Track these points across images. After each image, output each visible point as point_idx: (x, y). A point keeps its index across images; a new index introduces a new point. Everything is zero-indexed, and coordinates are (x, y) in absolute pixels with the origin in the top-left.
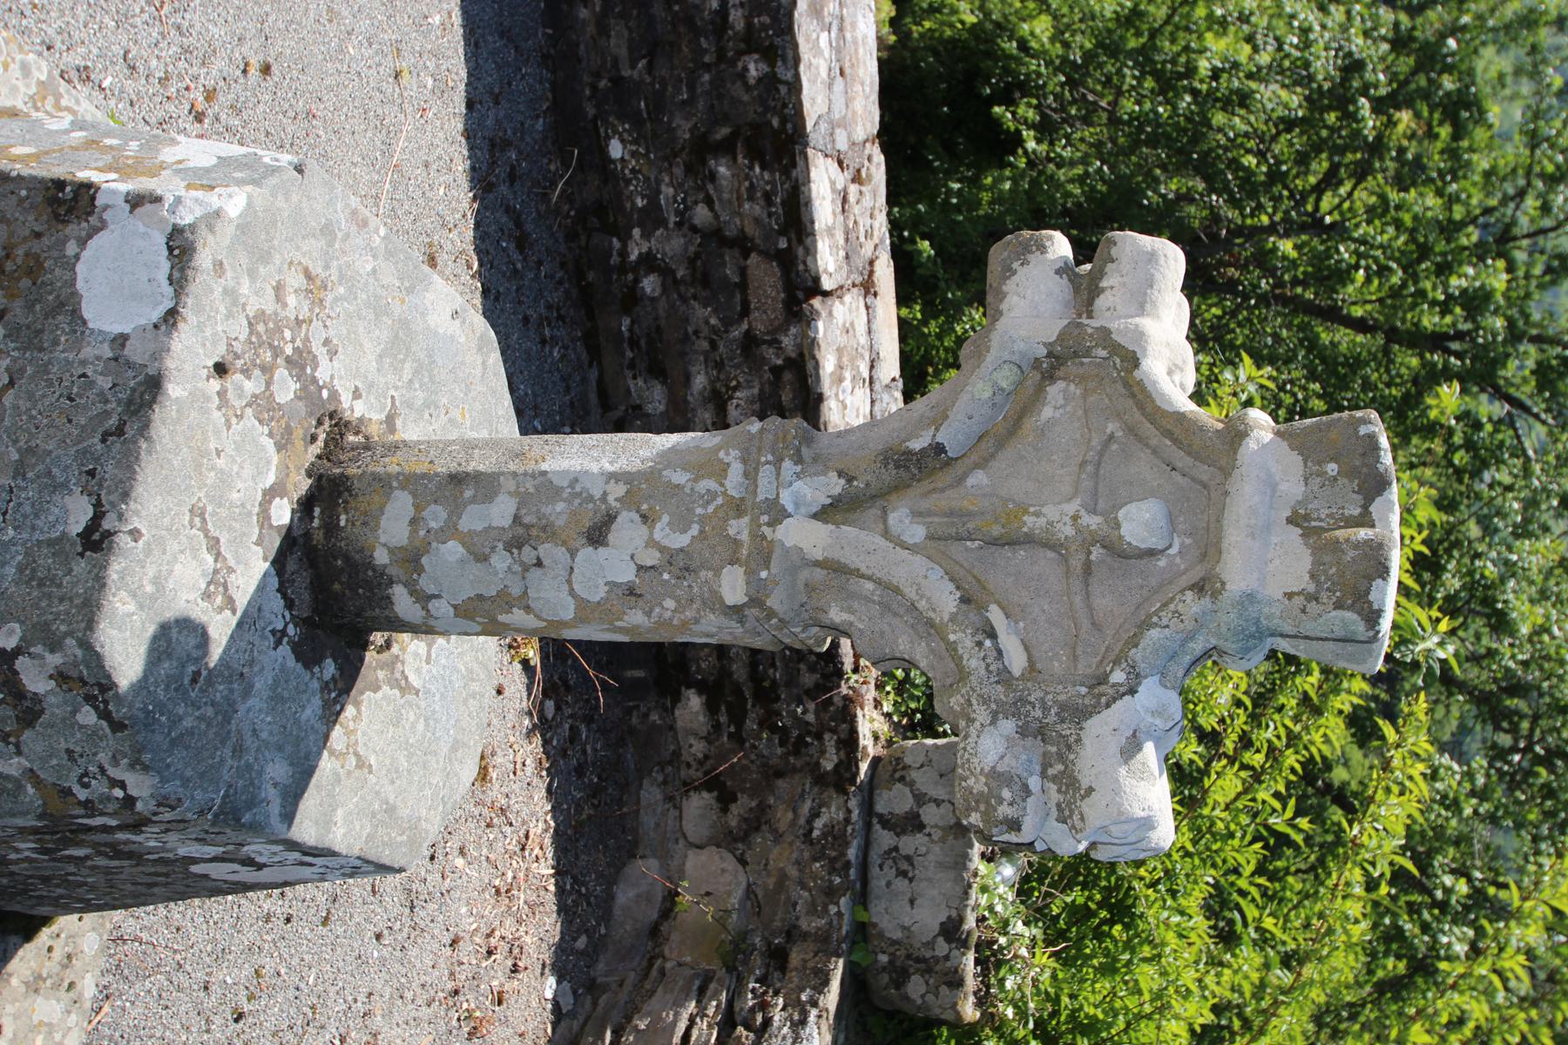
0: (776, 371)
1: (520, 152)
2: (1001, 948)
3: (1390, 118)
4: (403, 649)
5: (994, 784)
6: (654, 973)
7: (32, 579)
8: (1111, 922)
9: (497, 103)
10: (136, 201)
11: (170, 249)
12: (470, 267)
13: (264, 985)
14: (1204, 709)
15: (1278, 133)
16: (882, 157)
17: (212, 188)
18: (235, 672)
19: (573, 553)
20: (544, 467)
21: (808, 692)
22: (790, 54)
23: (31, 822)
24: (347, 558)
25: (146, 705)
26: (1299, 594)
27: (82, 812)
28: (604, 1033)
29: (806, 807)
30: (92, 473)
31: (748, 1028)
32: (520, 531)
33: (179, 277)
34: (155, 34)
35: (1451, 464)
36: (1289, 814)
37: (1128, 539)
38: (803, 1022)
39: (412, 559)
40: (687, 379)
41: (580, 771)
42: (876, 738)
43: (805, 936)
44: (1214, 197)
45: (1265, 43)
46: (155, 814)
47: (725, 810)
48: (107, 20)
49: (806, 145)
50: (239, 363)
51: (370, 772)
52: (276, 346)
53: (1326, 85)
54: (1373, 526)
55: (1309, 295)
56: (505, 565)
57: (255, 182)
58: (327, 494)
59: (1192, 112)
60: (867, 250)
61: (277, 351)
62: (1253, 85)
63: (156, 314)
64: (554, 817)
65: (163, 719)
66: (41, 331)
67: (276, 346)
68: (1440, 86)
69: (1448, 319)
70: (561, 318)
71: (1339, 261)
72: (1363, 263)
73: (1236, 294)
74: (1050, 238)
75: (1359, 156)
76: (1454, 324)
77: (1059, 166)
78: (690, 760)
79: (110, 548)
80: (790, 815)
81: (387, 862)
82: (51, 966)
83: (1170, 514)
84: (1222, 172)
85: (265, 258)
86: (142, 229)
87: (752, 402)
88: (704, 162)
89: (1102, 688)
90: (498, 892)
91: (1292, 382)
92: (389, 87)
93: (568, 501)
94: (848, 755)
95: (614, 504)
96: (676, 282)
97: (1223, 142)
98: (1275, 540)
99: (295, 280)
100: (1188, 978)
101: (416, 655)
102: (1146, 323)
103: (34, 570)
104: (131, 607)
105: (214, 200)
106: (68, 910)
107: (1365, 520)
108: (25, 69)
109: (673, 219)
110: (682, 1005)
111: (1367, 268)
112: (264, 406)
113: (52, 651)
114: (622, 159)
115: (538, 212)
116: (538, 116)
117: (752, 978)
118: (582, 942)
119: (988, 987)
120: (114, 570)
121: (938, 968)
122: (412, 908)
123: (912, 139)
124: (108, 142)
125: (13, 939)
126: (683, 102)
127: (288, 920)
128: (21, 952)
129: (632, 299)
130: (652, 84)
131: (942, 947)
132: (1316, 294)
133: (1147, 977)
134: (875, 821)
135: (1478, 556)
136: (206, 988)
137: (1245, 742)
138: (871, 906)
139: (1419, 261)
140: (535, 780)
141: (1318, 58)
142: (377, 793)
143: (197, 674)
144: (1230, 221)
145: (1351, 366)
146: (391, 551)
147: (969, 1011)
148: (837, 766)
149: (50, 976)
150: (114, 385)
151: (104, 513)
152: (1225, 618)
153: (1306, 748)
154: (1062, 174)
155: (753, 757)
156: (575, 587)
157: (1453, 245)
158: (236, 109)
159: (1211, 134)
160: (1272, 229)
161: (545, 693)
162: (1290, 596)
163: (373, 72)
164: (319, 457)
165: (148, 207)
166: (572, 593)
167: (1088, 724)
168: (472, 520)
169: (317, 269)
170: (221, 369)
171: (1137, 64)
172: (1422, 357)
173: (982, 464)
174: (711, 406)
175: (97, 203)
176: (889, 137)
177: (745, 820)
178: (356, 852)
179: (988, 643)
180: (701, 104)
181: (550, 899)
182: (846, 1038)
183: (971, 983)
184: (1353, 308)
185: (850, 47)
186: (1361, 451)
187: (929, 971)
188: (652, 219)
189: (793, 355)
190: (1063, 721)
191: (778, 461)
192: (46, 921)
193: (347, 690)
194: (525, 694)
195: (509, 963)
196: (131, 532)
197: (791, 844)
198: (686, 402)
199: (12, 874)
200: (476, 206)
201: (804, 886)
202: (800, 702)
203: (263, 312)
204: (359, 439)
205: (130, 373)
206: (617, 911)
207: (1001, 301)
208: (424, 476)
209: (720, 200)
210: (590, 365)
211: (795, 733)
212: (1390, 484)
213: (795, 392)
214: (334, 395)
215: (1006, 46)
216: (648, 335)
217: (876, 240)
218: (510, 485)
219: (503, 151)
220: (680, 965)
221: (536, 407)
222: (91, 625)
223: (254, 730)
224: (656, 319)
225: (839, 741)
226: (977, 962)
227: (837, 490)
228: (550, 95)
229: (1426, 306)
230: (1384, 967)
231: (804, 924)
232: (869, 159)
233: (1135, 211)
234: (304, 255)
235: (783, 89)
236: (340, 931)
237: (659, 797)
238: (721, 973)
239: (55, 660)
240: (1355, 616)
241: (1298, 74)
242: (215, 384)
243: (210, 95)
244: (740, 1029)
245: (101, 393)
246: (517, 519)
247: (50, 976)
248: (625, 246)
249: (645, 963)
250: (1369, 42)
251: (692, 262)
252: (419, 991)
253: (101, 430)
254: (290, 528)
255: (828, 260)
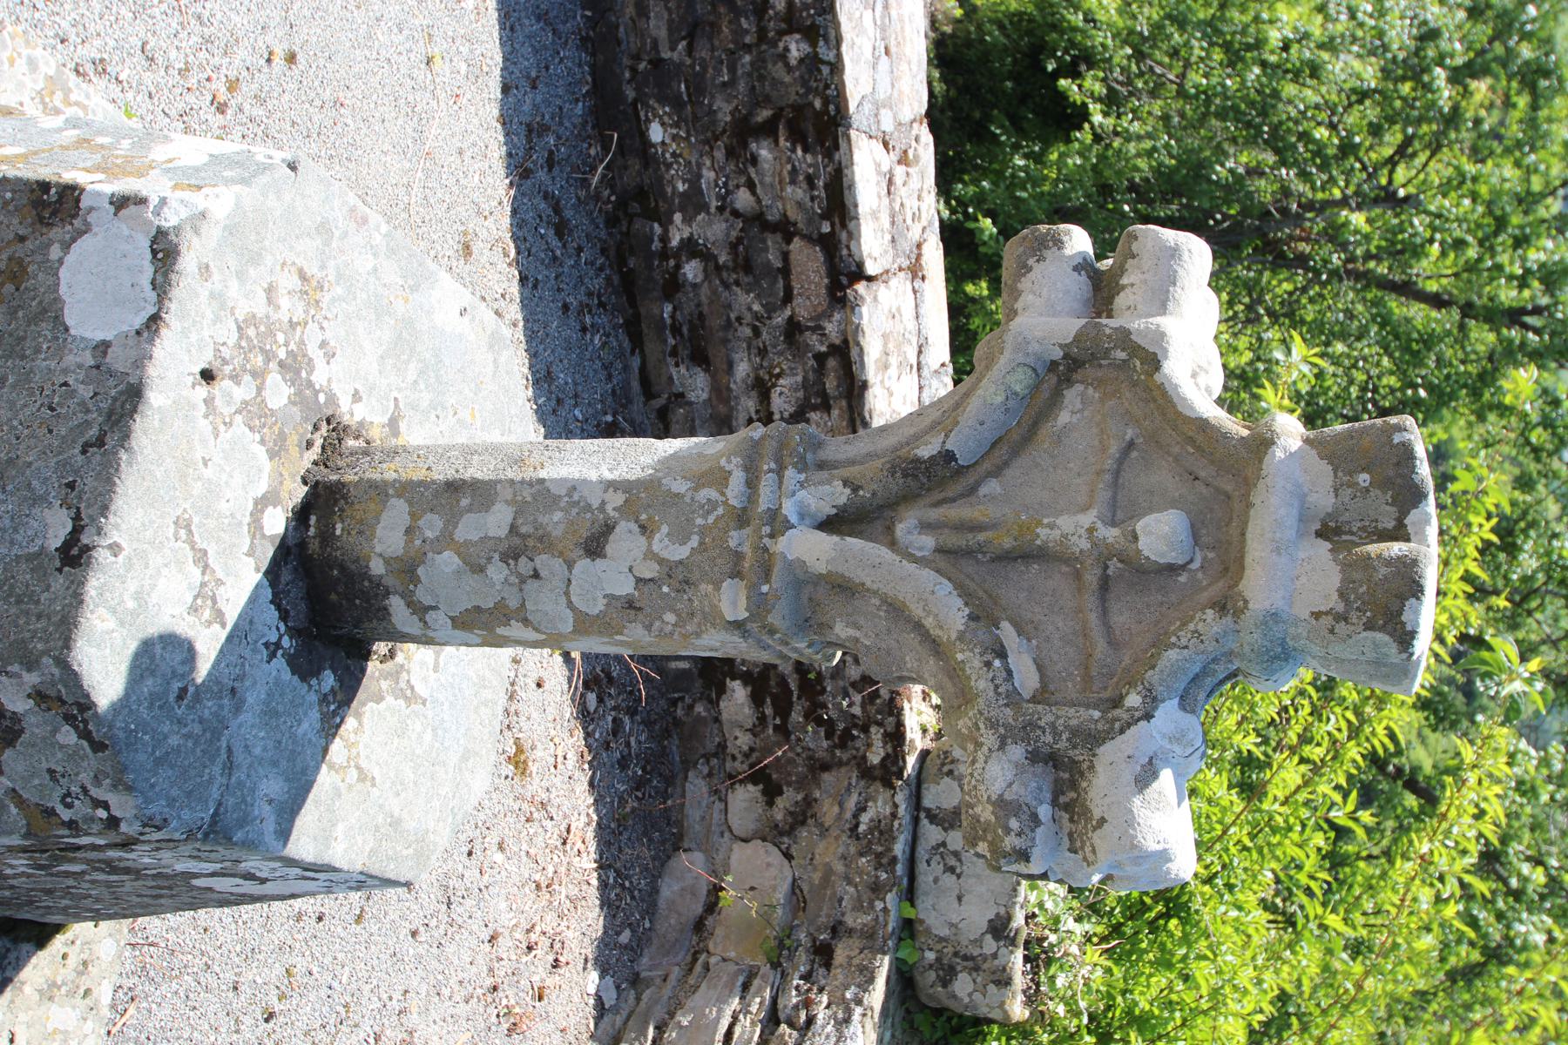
0: (820, 358)
1: (559, 137)
2: (1052, 946)
3: (1466, 88)
4: (408, 658)
5: (1001, 813)
6: (698, 968)
7: (10, 595)
8: (1167, 916)
9: (534, 87)
10: (121, 203)
11: (154, 252)
12: (506, 255)
13: (295, 985)
14: (1262, 699)
15: (1350, 105)
16: (931, 138)
17: (199, 188)
18: (228, 687)
19: (570, 565)
20: (543, 474)
21: (853, 685)
22: (832, 33)
23: (16, 841)
24: (342, 568)
25: (128, 724)
26: (1326, 613)
27: (67, 832)
28: (647, 1029)
29: (852, 802)
30: (71, 486)
31: (791, 1025)
32: (517, 541)
33: (161, 286)
34: (174, 25)
35: (1528, 442)
36: (1350, 807)
37: (1146, 553)
38: (847, 1020)
39: (408, 569)
40: (730, 365)
41: (623, 763)
42: (925, 731)
43: (850, 932)
44: (1284, 171)
45: (1338, 13)
46: (142, 834)
47: (770, 803)
48: (123, 11)
49: (849, 126)
50: (227, 369)
51: (374, 785)
52: (273, 351)
53: (1401, 56)
54: (1408, 540)
55: (1383, 270)
56: (502, 577)
57: (244, 181)
58: (322, 502)
59: (1262, 85)
60: (915, 234)
61: (268, 356)
62: (1325, 56)
63: (139, 321)
64: (597, 810)
65: (147, 737)
66: (24, 338)
67: (273, 351)
68: (1518, 55)
69: (1526, 293)
70: (601, 305)
71: (1415, 235)
72: (1438, 236)
73: (1307, 269)
74: (1068, 233)
75: (1434, 127)
76: (1533, 298)
77: (1128, 140)
78: (736, 752)
79: (88, 564)
80: (836, 809)
81: (392, 876)
82: (66, 973)
83: (1192, 526)
84: (1294, 147)
85: (255, 259)
86: (126, 232)
87: (796, 390)
88: (745, 145)
89: (1117, 712)
90: (538, 887)
91: (1365, 359)
92: (421, 73)
93: (566, 510)
94: (895, 748)
95: (612, 513)
96: (718, 268)
97: (1294, 113)
98: (1302, 555)
99: (289, 281)
100: (1245, 977)
101: (423, 663)
102: (1166, 323)
103: (12, 587)
104: (111, 624)
105: (199, 200)
106: (79, 918)
107: (1400, 533)
108: (32, 64)
109: (714, 204)
110: (725, 1002)
111: (1442, 243)
112: (255, 413)
113: (29, 670)
114: (663, 142)
115: (578, 199)
116: (577, 100)
117: (797, 975)
118: (625, 937)
119: (1038, 985)
120: (92, 588)
121: (985, 966)
122: (449, 904)
123: (977, 115)
124: (100, 140)
125: (25, 947)
126: (724, 84)
127: (320, 919)
128: (34, 960)
129: (673, 286)
130: (692, 66)
131: (990, 945)
132: (1390, 269)
133: (1203, 972)
134: (922, 815)
135: (1555, 536)
136: (235, 988)
137: (1305, 739)
138: (918, 902)
139: (1496, 234)
140: (577, 774)
141: (1393, 27)
142: (381, 806)
143: (184, 690)
144: (1300, 195)
145: (1425, 342)
146: (387, 561)
147: (1018, 1010)
148: (883, 760)
149: (64, 983)
150: (96, 394)
151: (83, 527)
152: (1248, 638)
153: (1368, 739)
154: (1132, 148)
155: (799, 750)
156: (574, 599)
157: (1531, 218)
158: (259, 99)
159: (1280, 106)
160: (1344, 202)
161: (586, 685)
162: (1317, 615)
163: (404, 58)
164: (315, 463)
165: (132, 208)
166: (570, 604)
167: (1101, 750)
168: (468, 529)
169: (312, 270)
170: (207, 376)
171: (1205, 36)
172: (1499, 334)
173: (997, 472)
174: (754, 394)
175: (82, 205)
176: (935, 117)
177: (791, 813)
178: (359, 868)
179: (997, 663)
180: (742, 86)
181: (593, 894)
182: (893, 1036)
183: (1020, 981)
184: (1428, 283)
185: (896, 25)
186: (1395, 460)
187: (977, 969)
188: (693, 203)
189: (837, 342)
190: (1074, 747)
191: (780, 472)
192: (58, 928)
193: (347, 702)
194: (566, 687)
195: (551, 958)
196: (110, 547)
197: (837, 838)
198: (729, 389)
199: (12, 887)
200: (512, 192)
201: (850, 882)
202: (846, 695)
203: (254, 316)
204: (361, 443)
205: (111, 382)
206: (662, 904)
207: (1016, 300)
208: (421, 483)
209: (761, 183)
210: (633, 352)
211: (841, 726)
212: (1426, 496)
213: (838, 382)
214: (332, 399)
215: (1072, 18)
216: (690, 322)
217: (924, 222)
218: (507, 494)
219: (540, 136)
220: (724, 960)
221: (576, 396)
222: (67, 643)
223: (246, 746)
224: (698, 305)
225: (886, 735)
226: (1027, 959)
227: (842, 500)
228: (589, 79)
229: (1503, 281)
230: (1458, 955)
231: (849, 920)
232: (917, 140)
233: (1205, 186)
234: (298, 255)
235: (825, 70)
236: (374, 929)
237: (705, 790)
238: (766, 969)
239: (32, 679)
240: (1387, 638)
241: (1378, 47)
242: (202, 391)
243: (233, 86)
244: (783, 1027)
245: (83, 404)
246: (513, 529)
247: (64, 983)
248: (666, 231)
249: (689, 958)
250: (1445, 10)
251: (734, 247)
252: (456, 987)
253: (81, 441)
254: (284, 538)
255: (873, 244)
